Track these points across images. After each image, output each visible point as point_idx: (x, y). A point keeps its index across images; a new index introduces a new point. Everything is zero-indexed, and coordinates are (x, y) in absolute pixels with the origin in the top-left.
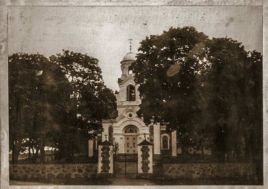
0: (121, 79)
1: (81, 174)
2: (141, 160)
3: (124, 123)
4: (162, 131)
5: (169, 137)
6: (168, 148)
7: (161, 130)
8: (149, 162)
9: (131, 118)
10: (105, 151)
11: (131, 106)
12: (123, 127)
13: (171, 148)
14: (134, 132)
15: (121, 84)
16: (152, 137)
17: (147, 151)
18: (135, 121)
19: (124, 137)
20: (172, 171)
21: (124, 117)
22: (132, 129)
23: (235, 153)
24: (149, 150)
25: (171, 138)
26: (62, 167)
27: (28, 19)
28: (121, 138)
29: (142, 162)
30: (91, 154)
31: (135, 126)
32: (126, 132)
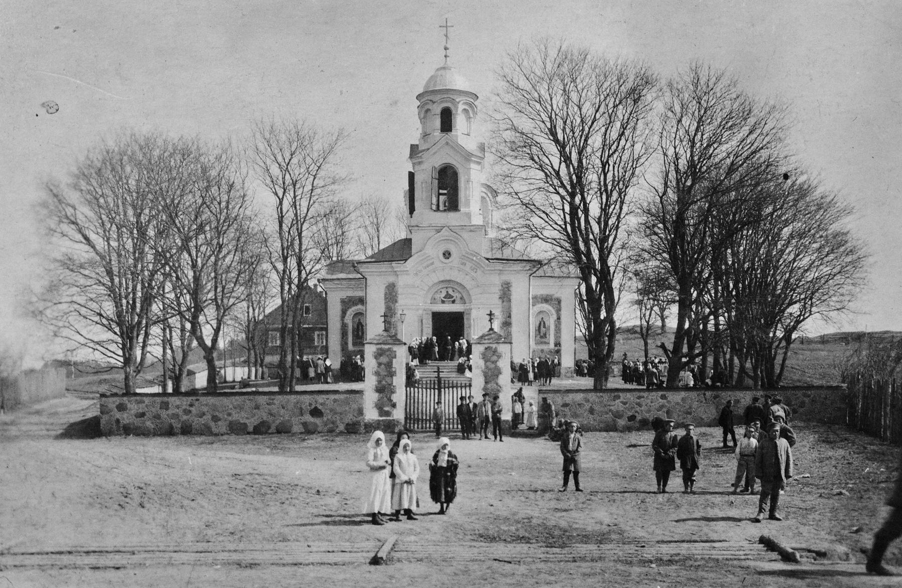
1: (318, 421)
10: (384, 359)
13: (558, 344)
17: (495, 358)
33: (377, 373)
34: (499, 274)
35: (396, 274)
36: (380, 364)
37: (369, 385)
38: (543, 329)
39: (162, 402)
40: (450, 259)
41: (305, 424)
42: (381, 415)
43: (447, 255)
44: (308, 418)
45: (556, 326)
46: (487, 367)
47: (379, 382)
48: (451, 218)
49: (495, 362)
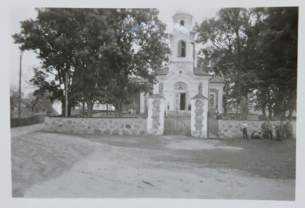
0: (173, 35)
1: (129, 130)
2: (195, 116)
4: (210, 89)
5: (215, 96)
6: (213, 106)
7: (210, 88)
8: (203, 118)
9: (181, 75)
10: (156, 105)
11: (181, 62)
12: (175, 83)
13: (217, 106)
14: (183, 89)
15: (172, 40)
17: (201, 105)
19: (173, 94)
20: (229, 129)
21: (174, 74)
22: (182, 86)
23: (36, 146)
24: (203, 105)
25: (217, 97)
26: (109, 122)
27: (120, 83)
28: (171, 95)
29: (196, 119)
30: (142, 111)
31: (184, 83)
32: (175, 89)
33: (153, 110)
34: (199, 80)
35: (163, 79)
36: (154, 107)
37: (150, 120)
38: (212, 101)
39: (69, 121)
40: (182, 74)
41: (123, 131)
42: (159, 101)
43: (181, 72)
44: (125, 129)
45: (216, 99)
46: (197, 109)
47: (154, 114)
48: (182, 59)
49: (201, 107)
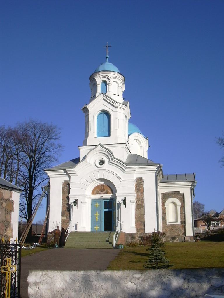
3: (114, 174)
16: (65, 218)
18: (109, 171)
